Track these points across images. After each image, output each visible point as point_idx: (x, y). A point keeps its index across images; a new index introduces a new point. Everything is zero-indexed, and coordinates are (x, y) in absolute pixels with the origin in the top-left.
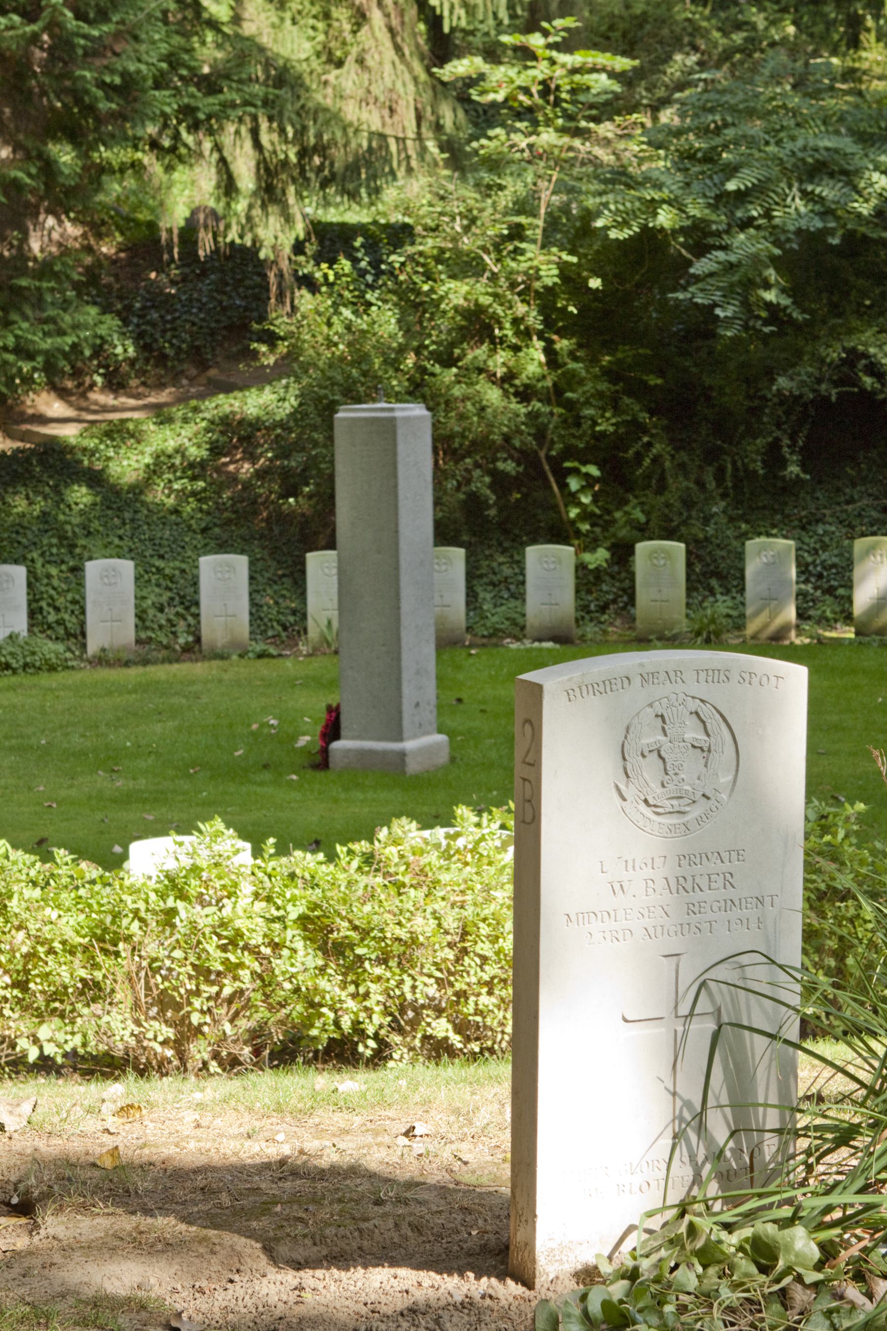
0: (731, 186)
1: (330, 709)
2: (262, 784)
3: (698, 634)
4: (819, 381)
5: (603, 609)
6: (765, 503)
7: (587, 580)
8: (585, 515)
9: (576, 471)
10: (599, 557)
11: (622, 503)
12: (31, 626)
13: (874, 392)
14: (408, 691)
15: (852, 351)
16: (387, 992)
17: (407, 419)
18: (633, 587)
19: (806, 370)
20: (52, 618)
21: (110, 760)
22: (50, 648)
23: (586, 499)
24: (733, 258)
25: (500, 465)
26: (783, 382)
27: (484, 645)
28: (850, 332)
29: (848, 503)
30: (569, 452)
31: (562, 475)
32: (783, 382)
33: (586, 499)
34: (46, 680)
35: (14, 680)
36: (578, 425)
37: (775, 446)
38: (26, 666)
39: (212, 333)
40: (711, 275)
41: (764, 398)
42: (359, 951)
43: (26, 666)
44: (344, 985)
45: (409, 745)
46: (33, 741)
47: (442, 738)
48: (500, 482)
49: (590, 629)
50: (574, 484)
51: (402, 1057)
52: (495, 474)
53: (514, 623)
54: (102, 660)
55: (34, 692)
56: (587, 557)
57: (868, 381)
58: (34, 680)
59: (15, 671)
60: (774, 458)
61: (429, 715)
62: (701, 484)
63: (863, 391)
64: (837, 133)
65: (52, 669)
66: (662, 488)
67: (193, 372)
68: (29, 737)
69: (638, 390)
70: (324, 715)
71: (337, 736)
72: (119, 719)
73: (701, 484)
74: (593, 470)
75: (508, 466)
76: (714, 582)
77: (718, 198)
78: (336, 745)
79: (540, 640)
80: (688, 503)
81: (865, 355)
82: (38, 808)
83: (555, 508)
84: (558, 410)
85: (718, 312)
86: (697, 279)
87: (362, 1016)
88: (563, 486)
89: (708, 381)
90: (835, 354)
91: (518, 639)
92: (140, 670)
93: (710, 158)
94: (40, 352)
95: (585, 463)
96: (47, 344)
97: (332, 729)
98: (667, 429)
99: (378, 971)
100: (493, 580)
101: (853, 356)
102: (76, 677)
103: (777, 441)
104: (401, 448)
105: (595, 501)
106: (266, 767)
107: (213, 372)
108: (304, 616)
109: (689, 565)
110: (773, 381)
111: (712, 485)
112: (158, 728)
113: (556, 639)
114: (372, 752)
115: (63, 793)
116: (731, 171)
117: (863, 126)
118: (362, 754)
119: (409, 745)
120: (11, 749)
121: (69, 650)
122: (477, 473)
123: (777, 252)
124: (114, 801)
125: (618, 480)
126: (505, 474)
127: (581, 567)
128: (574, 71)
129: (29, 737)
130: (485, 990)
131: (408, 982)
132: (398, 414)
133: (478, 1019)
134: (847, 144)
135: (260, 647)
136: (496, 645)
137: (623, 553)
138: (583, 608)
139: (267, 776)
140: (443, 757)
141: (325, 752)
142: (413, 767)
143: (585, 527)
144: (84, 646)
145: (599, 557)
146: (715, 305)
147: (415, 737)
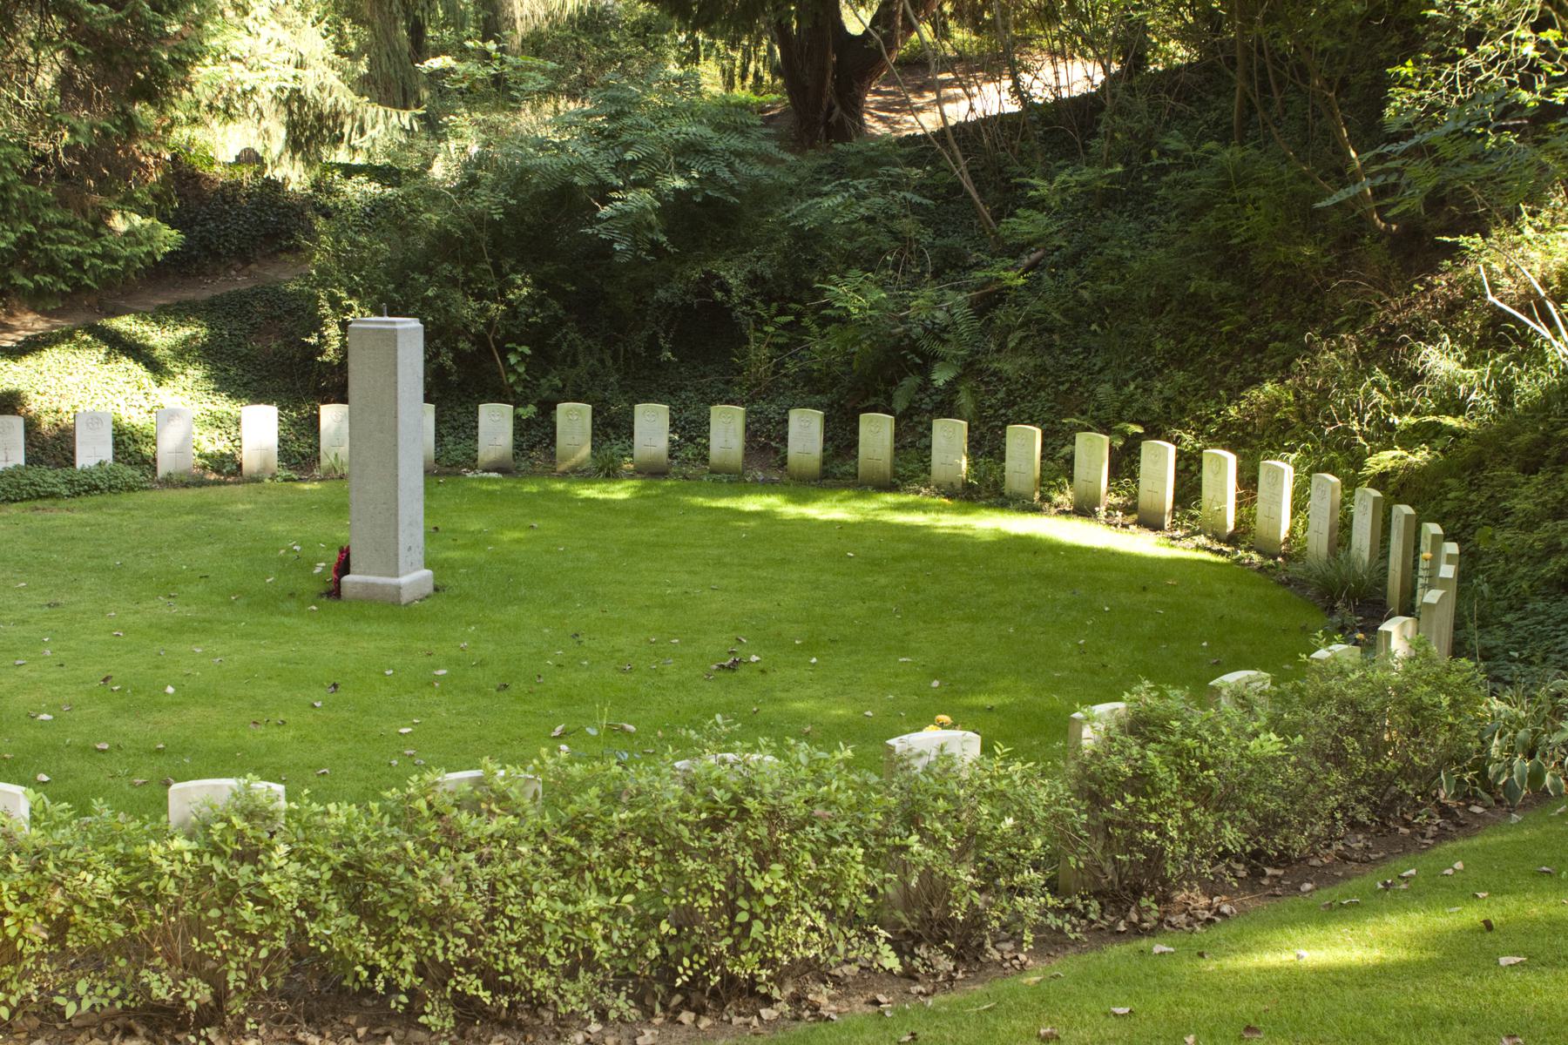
0: (629, 156)
1: (342, 551)
2: (289, 614)
3: (601, 470)
4: (686, 293)
5: (532, 448)
6: (648, 382)
7: (521, 427)
8: (520, 380)
9: (515, 350)
10: (529, 411)
11: (545, 373)
12: (115, 455)
13: (722, 303)
14: (403, 539)
15: (708, 273)
16: (417, 950)
17: (406, 330)
18: (554, 433)
19: (678, 286)
20: (131, 449)
21: (168, 585)
22: (129, 472)
23: (521, 369)
24: (627, 208)
25: (461, 345)
26: (661, 293)
27: (448, 474)
28: (706, 260)
29: (702, 377)
30: (509, 337)
31: (504, 354)
32: (661, 293)
33: (521, 369)
34: (127, 499)
35: (101, 499)
36: (516, 318)
37: (655, 335)
38: (111, 487)
39: (254, 238)
40: (611, 218)
41: (646, 303)
42: (393, 913)
43: (111, 487)
44: (377, 947)
45: (403, 580)
46: (110, 562)
47: (428, 572)
48: (459, 356)
49: (524, 465)
50: (513, 359)
51: (433, 1010)
52: (455, 350)
53: (468, 456)
54: (169, 482)
55: (115, 511)
56: (521, 411)
57: (719, 294)
58: (116, 499)
59: (102, 491)
60: (653, 345)
61: (418, 556)
62: (602, 361)
63: (715, 302)
64: (701, 123)
65: (131, 489)
66: (575, 363)
67: (240, 266)
68: (107, 557)
69: (557, 293)
70: (337, 553)
71: (348, 572)
72: (178, 541)
73: (602, 361)
74: (526, 350)
75: (464, 345)
76: (609, 430)
77: (617, 163)
78: (346, 578)
79: (487, 471)
80: (593, 375)
81: (717, 277)
82: (107, 637)
83: (499, 374)
84: (502, 307)
85: (617, 247)
86: (600, 221)
87: (395, 974)
88: (505, 360)
89: (608, 289)
90: (697, 275)
91: (472, 469)
92: (197, 491)
93: (612, 136)
94: (120, 258)
95: (520, 344)
96: (127, 252)
97: (344, 567)
98: (578, 322)
99: (410, 930)
100: (455, 426)
101: (710, 277)
102: (150, 495)
103: (655, 334)
104: (400, 353)
105: (526, 371)
106: (292, 595)
107: (253, 267)
108: (318, 449)
109: (593, 417)
110: (654, 291)
111: (609, 362)
112: (208, 550)
113: (497, 470)
114: (374, 585)
115: (130, 619)
116: (628, 146)
117: (719, 119)
118: (367, 586)
119: (403, 580)
120: (93, 570)
121: (143, 474)
122: (444, 350)
123: (658, 204)
124: (169, 630)
125: (544, 357)
126: (463, 350)
127: (517, 417)
128: (516, 68)
129: (107, 557)
130: (513, 950)
131: (440, 943)
132: (398, 326)
133: (508, 978)
134: (709, 132)
135: (285, 473)
136: (458, 474)
137: (547, 409)
138: (517, 446)
139: (291, 605)
140: (429, 589)
141: (338, 582)
142: (405, 598)
143: (519, 389)
144: (155, 470)
145: (529, 411)
146: (612, 241)
147: (408, 573)
